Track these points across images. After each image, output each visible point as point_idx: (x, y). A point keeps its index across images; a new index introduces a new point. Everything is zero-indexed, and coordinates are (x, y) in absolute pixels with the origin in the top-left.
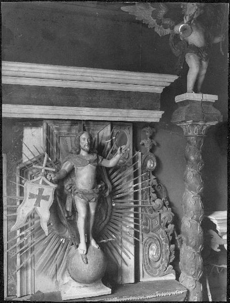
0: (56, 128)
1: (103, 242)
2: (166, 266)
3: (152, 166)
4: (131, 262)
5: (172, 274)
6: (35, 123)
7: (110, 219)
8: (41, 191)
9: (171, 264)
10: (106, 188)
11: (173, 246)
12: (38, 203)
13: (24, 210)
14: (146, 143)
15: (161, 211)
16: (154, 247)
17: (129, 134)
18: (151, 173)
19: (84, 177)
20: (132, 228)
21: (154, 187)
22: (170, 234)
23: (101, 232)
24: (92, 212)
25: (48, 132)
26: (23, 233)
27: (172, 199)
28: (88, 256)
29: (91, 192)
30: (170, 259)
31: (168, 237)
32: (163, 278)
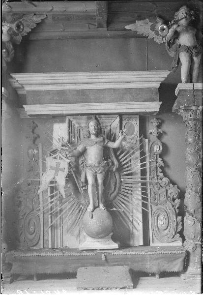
0: (77, 123)
1: (113, 210)
2: (174, 234)
3: (158, 149)
4: (140, 227)
5: (179, 241)
6: (60, 118)
7: (119, 190)
8: (58, 164)
9: (179, 233)
10: (113, 163)
11: (180, 218)
12: (56, 174)
13: (46, 178)
14: (152, 129)
15: (168, 187)
16: (161, 217)
17: (136, 124)
18: (158, 156)
19: (93, 154)
20: (139, 200)
21: (161, 167)
22: (176, 208)
23: (109, 201)
24: (100, 181)
25: (70, 125)
26: (52, 200)
27: (174, 178)
28: (93, 213)
29: (97, 165)
30: (177, 229)
31: (175, 210)
32: (171, 244)
